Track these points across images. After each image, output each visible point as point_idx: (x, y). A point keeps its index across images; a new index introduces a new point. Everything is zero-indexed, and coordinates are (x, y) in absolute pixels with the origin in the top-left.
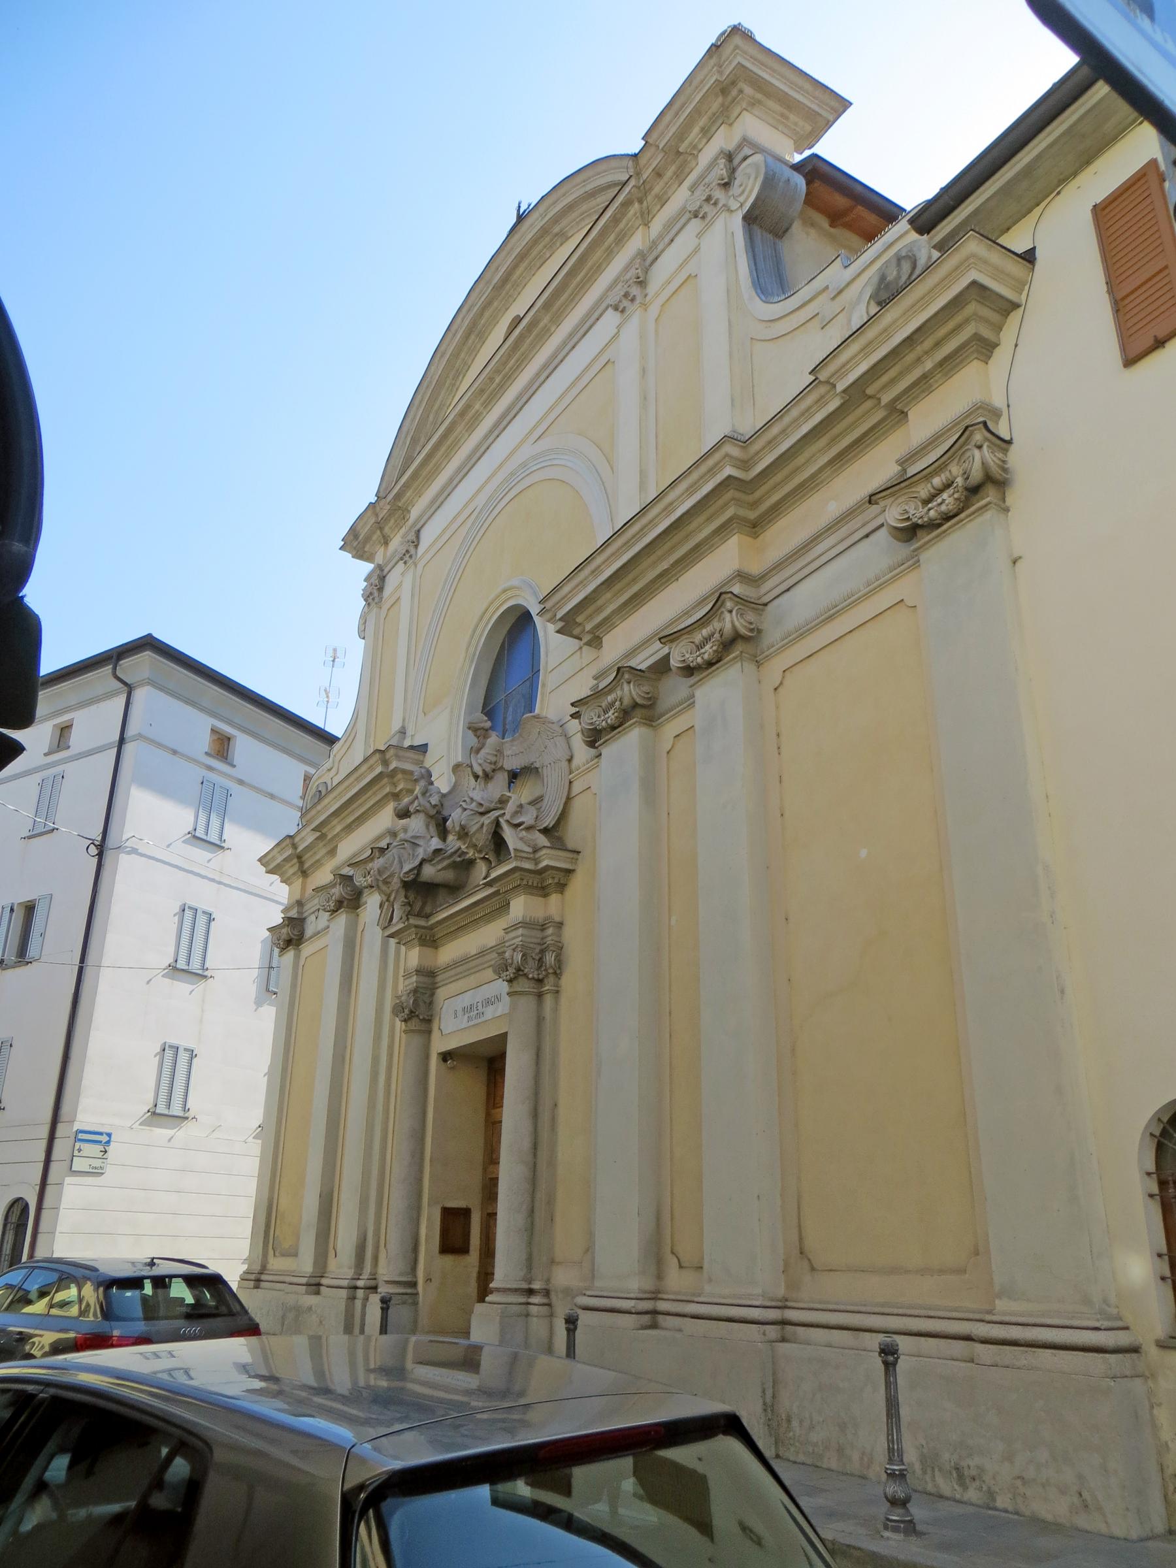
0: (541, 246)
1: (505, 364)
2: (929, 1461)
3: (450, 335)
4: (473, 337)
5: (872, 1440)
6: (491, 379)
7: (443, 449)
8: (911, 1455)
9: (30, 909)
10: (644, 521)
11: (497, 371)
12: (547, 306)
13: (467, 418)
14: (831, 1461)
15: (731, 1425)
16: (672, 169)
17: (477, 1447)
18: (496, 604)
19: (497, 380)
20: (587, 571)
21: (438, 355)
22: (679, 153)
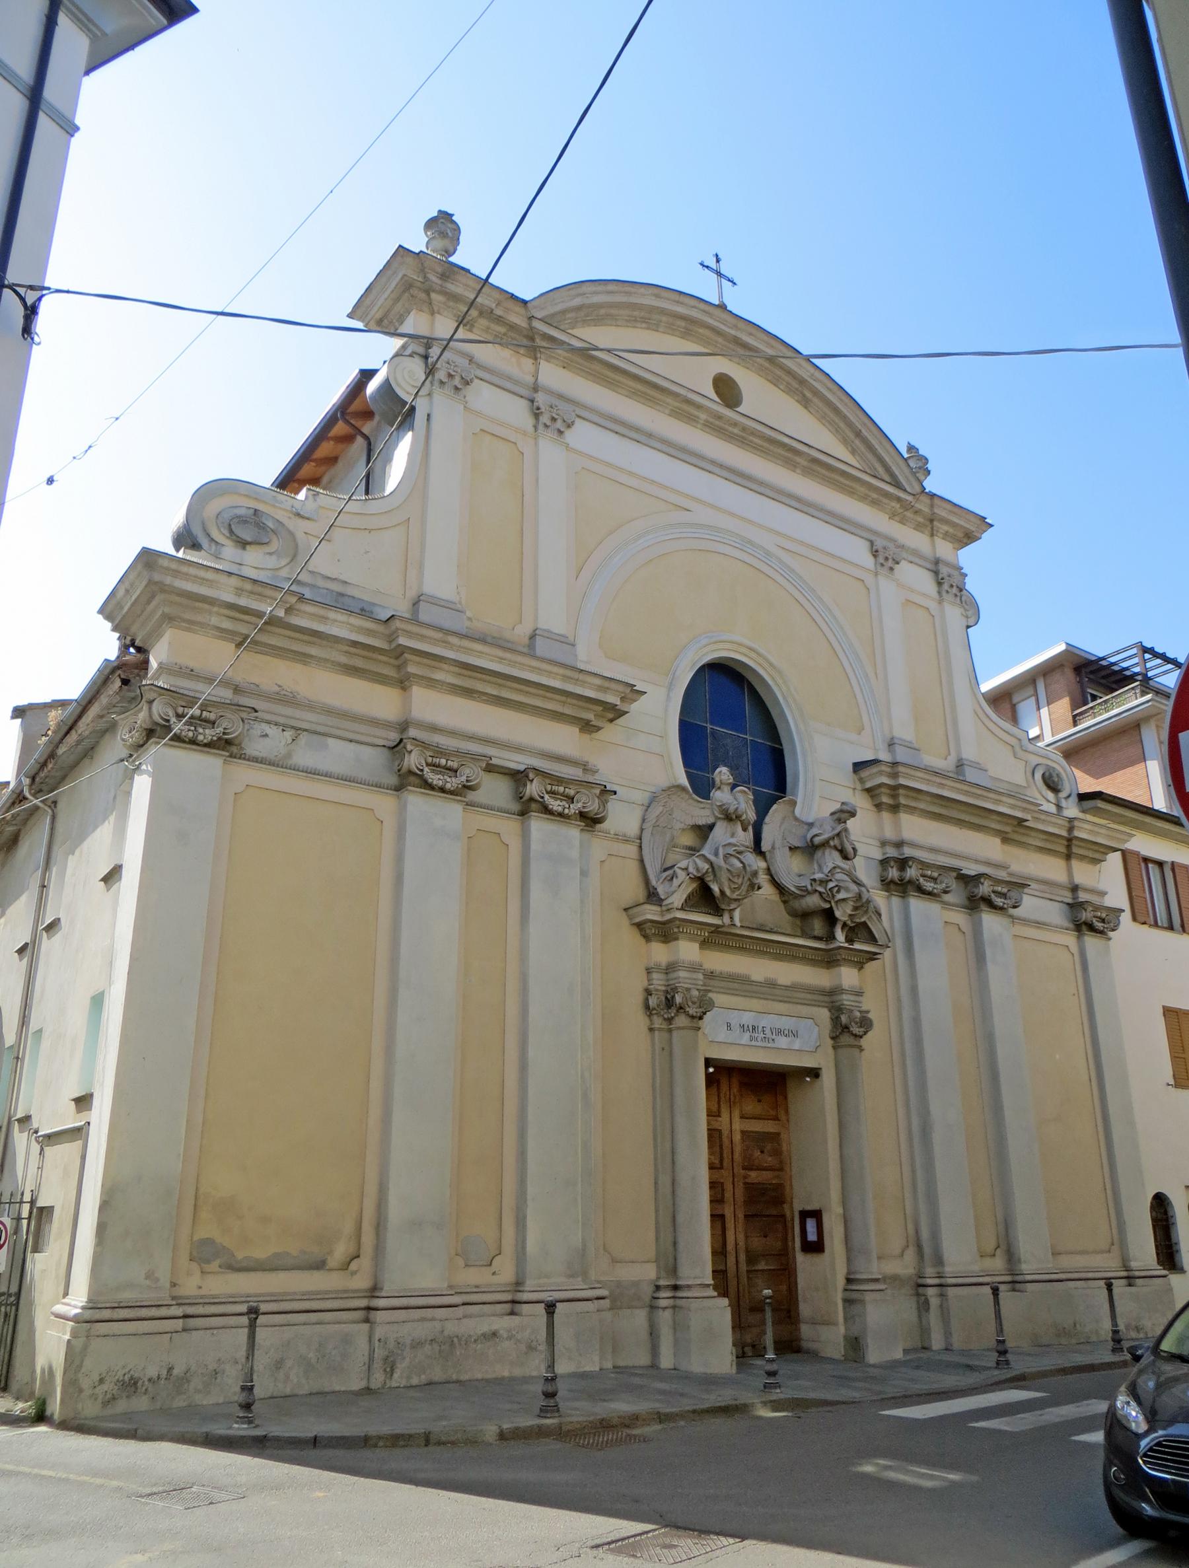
0: (786, 378)
1: (752, 434)
2: (1128, 1327)
3: (676, 297)
4: (683, 324)
5: (1107, 1325)
6: (735, 424)
7: (639, 387)
8: (1121, 1327)
9: (790, 848)
10: (985, 794)
11: (744, 429)
12: (815, 461)
13: (685, 407)
14: (1094, 1338)
15: (66, 1294)
16: (921, 520)
17: (780, 1417)
18: (766, 665)
19: (736, 431)
20: (938, 780)
21: (656, 291)
22: (932, 521)
